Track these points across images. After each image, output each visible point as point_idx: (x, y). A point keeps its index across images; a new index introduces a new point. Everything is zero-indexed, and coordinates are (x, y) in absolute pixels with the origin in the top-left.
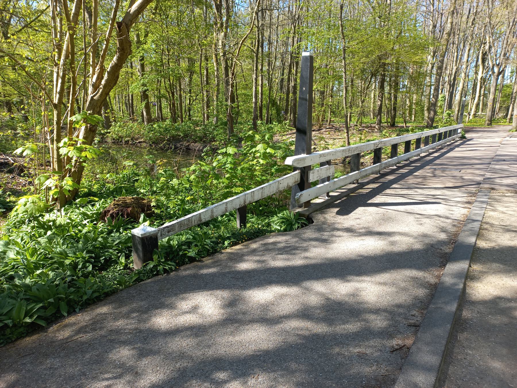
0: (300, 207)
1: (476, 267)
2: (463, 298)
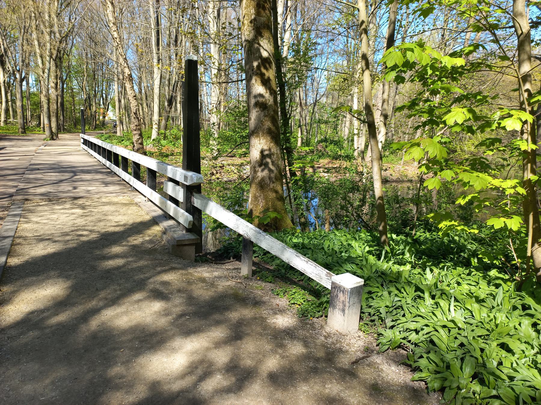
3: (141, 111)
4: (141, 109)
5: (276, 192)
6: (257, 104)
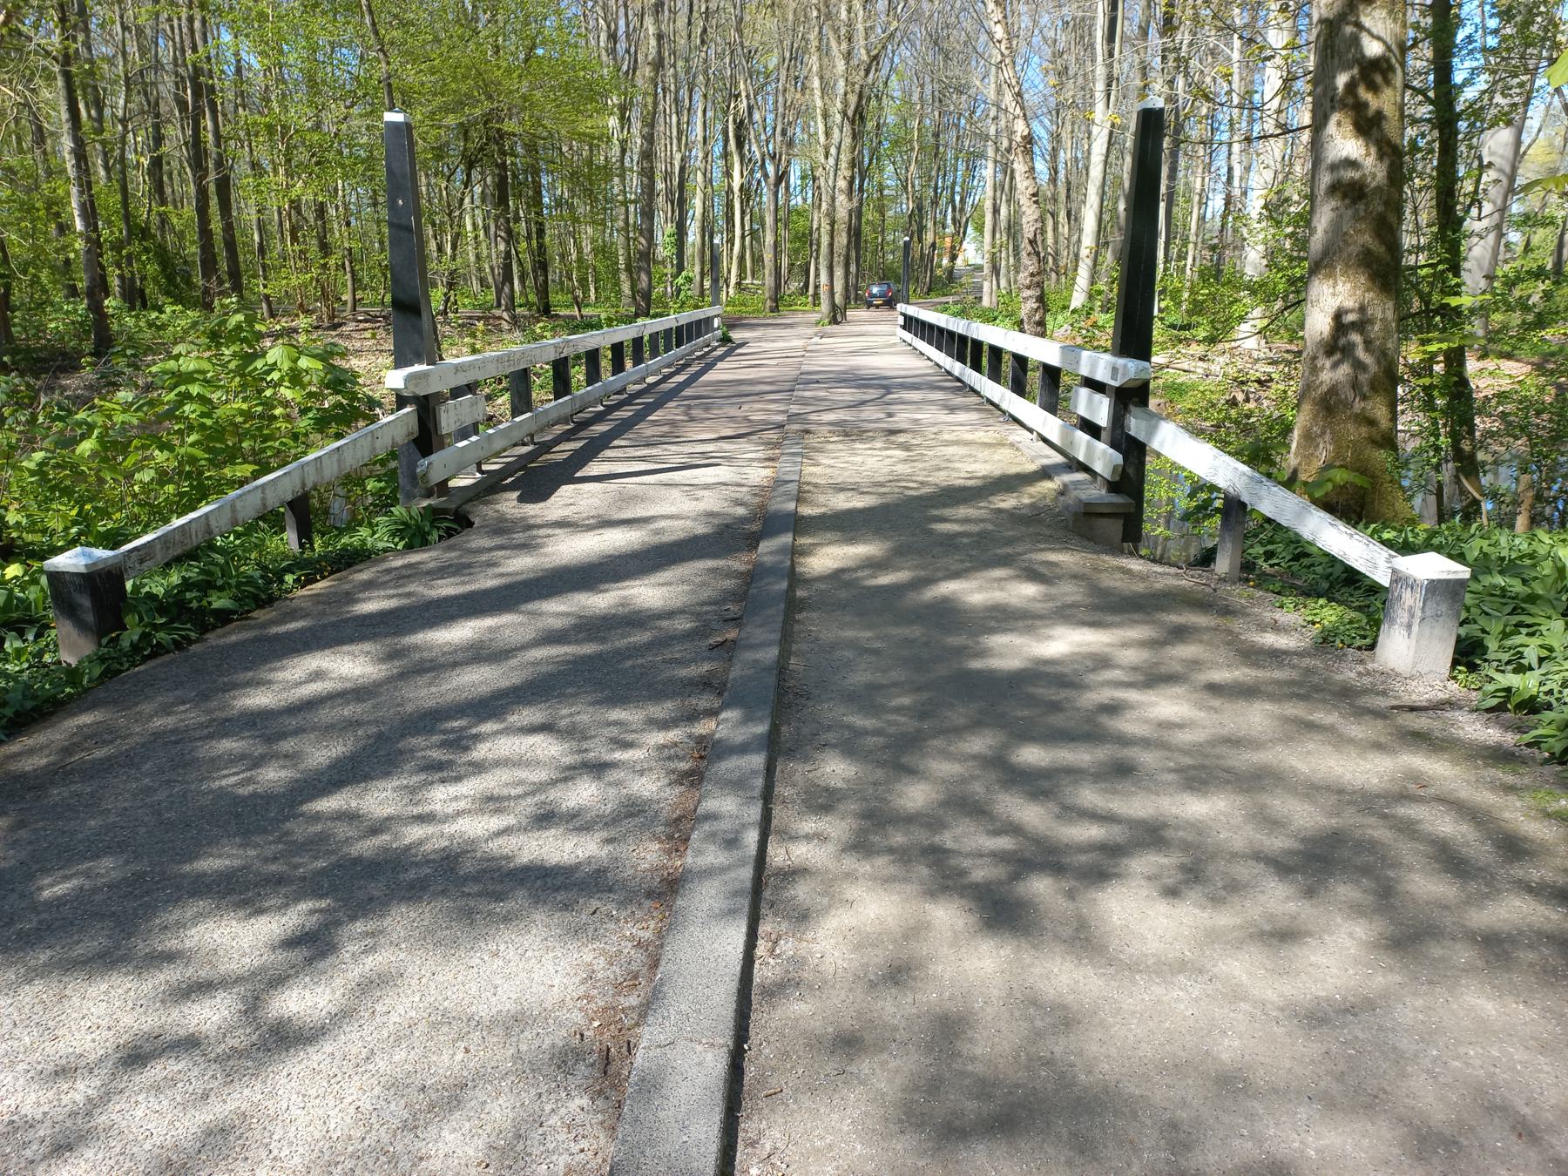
0: (429, 495)
1: (804, 541)
2: (795, 578)
3: (1050, 234)
4: (1050, 228)
5: (1371, 422)
6: (1334, 189)
